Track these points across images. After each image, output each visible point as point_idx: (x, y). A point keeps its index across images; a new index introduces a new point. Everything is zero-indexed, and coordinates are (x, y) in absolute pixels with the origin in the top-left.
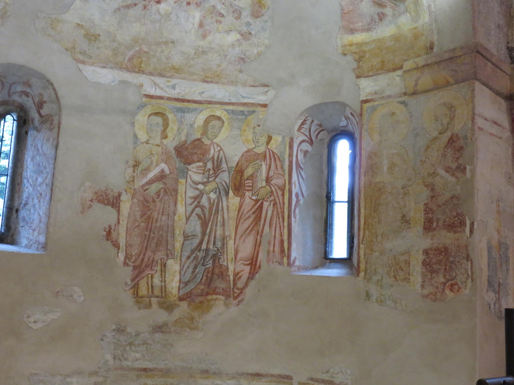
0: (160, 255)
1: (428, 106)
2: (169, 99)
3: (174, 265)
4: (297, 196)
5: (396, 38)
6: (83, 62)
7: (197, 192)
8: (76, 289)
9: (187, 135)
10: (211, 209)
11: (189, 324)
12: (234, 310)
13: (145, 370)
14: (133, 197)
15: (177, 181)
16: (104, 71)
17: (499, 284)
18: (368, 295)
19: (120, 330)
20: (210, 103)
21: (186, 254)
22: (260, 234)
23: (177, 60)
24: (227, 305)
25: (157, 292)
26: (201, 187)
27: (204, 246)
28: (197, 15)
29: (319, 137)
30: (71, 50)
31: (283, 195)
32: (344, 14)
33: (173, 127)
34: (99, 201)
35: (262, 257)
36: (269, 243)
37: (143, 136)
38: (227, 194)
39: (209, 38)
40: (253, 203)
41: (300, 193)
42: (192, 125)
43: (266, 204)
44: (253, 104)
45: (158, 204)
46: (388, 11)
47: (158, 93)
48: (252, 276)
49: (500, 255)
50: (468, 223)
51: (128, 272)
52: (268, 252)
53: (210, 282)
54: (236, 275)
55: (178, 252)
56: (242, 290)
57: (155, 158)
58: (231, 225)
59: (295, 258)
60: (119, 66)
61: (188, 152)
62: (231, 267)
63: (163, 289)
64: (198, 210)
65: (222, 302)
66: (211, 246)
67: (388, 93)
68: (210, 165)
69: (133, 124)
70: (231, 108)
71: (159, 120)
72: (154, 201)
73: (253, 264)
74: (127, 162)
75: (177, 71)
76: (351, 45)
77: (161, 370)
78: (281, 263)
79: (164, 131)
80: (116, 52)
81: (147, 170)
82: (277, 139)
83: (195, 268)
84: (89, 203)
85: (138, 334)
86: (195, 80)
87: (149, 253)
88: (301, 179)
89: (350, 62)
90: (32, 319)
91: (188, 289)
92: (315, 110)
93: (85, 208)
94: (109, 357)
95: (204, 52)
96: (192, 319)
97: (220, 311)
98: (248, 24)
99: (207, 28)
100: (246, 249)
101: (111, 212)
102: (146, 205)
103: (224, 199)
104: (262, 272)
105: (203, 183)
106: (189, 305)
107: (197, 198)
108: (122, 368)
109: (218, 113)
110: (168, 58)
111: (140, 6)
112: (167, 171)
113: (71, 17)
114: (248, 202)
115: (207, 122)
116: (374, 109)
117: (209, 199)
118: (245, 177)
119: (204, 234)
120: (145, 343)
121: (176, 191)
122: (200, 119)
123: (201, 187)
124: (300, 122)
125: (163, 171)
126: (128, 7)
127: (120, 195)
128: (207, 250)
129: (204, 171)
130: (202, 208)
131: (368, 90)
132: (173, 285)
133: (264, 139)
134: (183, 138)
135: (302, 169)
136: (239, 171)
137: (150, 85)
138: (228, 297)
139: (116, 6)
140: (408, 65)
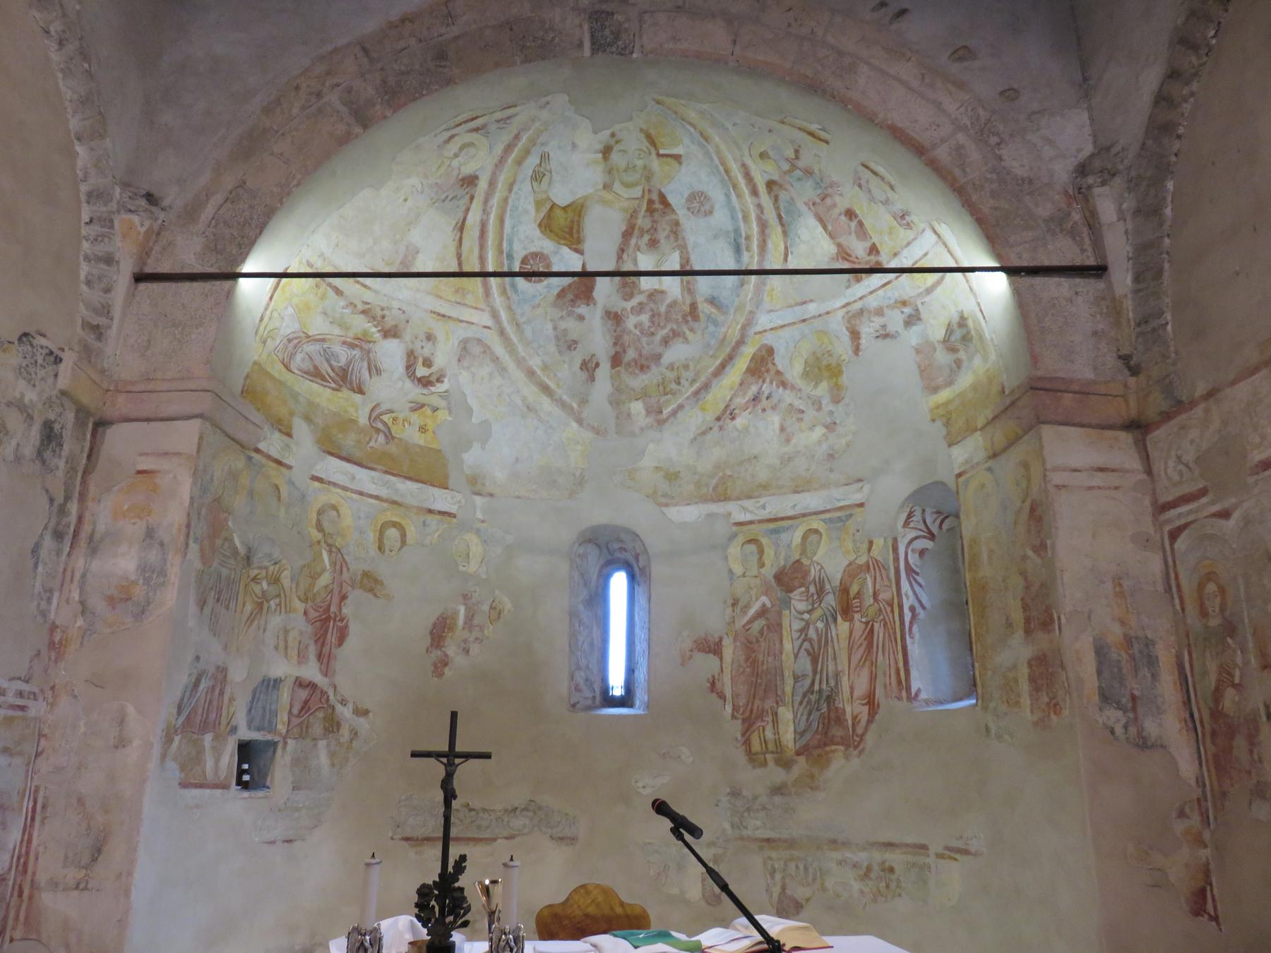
0: (769, 703)
1: (1009, 465)
2: (760, 522)
3: (786, 714)
4: (912, 609)
5: (974, 387)
6: (666, 505)
7: (803, 623)
8: (684, 749)
9: (786, 559)
10: (820, 641)
11: (810, 783)
12: (855, 762)
13: (768, 840)
14: (735, 640)
15: (780, 615)
16: (688, 508)
17: (1134, 698)
18: (987, 729)
19: (735, 794)
20: (804, 515)
21: (798, 699)
22: (874, 664)
23: (763, 475)
24: (847, 757)
25: (771, 747)
26: (806, 616)
27: (816, 687)
28: (775, 419)
29: (945, 526)
30: (652, 496)
31: (892, 611)
32: (923, 371)
33: (769, 552)
34: (699, 650)
35: (879, 692)
36: (885, 674)
37: (738, 569)
38: (835, 620)
39: (793, 441)
40: (863, 626)
41: (917, 605)
42: (789, 546)
43: (876, 626)
44: (849, 506)
45: (763, 644)
46: (962, 355)
47: (749, 517)
48: (871, 720)
49: (1133, 658)
50: (1055, 617)
51: (736, 728)
52: (885, 686)
53: (829, 731)
54: (855, 718)
55: (788, 698)
56: (862, 737)
57: (753, 592)
58: (843, 656)
59: (919, 691)
60: (705, 500)
61: (789, 578)
62: (848, 709)
63: (778, 742)
64: (806, 645)
65: (841, 754)
66: (824, 686)
67: (975, 461)
68: (812, 589)
69: (726, 558)
70: (827, 516)
71: (753, 548)
72: (758, 641)
73: (871, 701)
74: (725, 602)
75: (765, 487)
76: (938, 407)
77: (785, 841)
78: (900, 698)
79: (760, 558)
80: (698, 484)
81: (747, 606)
82: (879, 543)
83: (810, 714)
84: (688, 654)
85: (755, 798)
86: (784, 494)
87: (757, 702)
88: (917, 588)
89: (938, 429)
90: (640, 784)
91: (803, 741)
92: (919, 496)
93: (685, 660)
94: (727, 826)
95: (790, 459)
96: (812, 777)
97: (840, 765)
98: (831, 413)
99: (789, 430)
100: (862, 687)
101: (712, 660)
102: (749, 646)
103: (833, 626)
104: (881, 711)
105: (809, 612)
106: (807, 760)
107: (804, 630)
108: (742, 838)
109: (815, 526)
110: (753, 476)
111: (716, 429)
112: (769, 604)
113: (647, 463)
114: (859, 626)
115: (804, 538)
116: (967, 483)
117: (817, 630)
118: (852, 596)
119: (815, 672)
120: (764, 808)
121: (780, 625)
122: (797, 537)
123: (806, 616)
124: (904, 516)
125: (764, 605)
126: (704, 433)
127: (721, 639)
128: (820, 691)
129: (808, 596)
130: (810, 641)
131: (961, 459)
132: (788, 737)
133: (865, 546)
134: (782, 563)
135: (917, 574)
136: (844, 590)
137: (738, 511)
138: (848, 747)
139: (692, 436)
140: (980, 422)
